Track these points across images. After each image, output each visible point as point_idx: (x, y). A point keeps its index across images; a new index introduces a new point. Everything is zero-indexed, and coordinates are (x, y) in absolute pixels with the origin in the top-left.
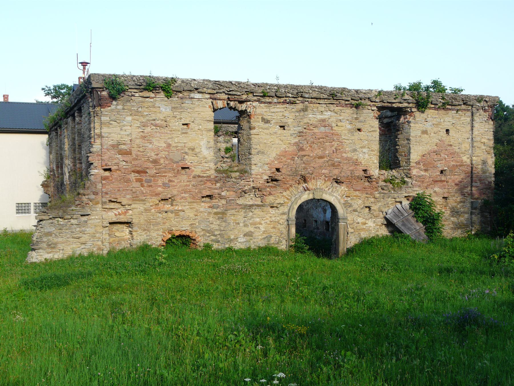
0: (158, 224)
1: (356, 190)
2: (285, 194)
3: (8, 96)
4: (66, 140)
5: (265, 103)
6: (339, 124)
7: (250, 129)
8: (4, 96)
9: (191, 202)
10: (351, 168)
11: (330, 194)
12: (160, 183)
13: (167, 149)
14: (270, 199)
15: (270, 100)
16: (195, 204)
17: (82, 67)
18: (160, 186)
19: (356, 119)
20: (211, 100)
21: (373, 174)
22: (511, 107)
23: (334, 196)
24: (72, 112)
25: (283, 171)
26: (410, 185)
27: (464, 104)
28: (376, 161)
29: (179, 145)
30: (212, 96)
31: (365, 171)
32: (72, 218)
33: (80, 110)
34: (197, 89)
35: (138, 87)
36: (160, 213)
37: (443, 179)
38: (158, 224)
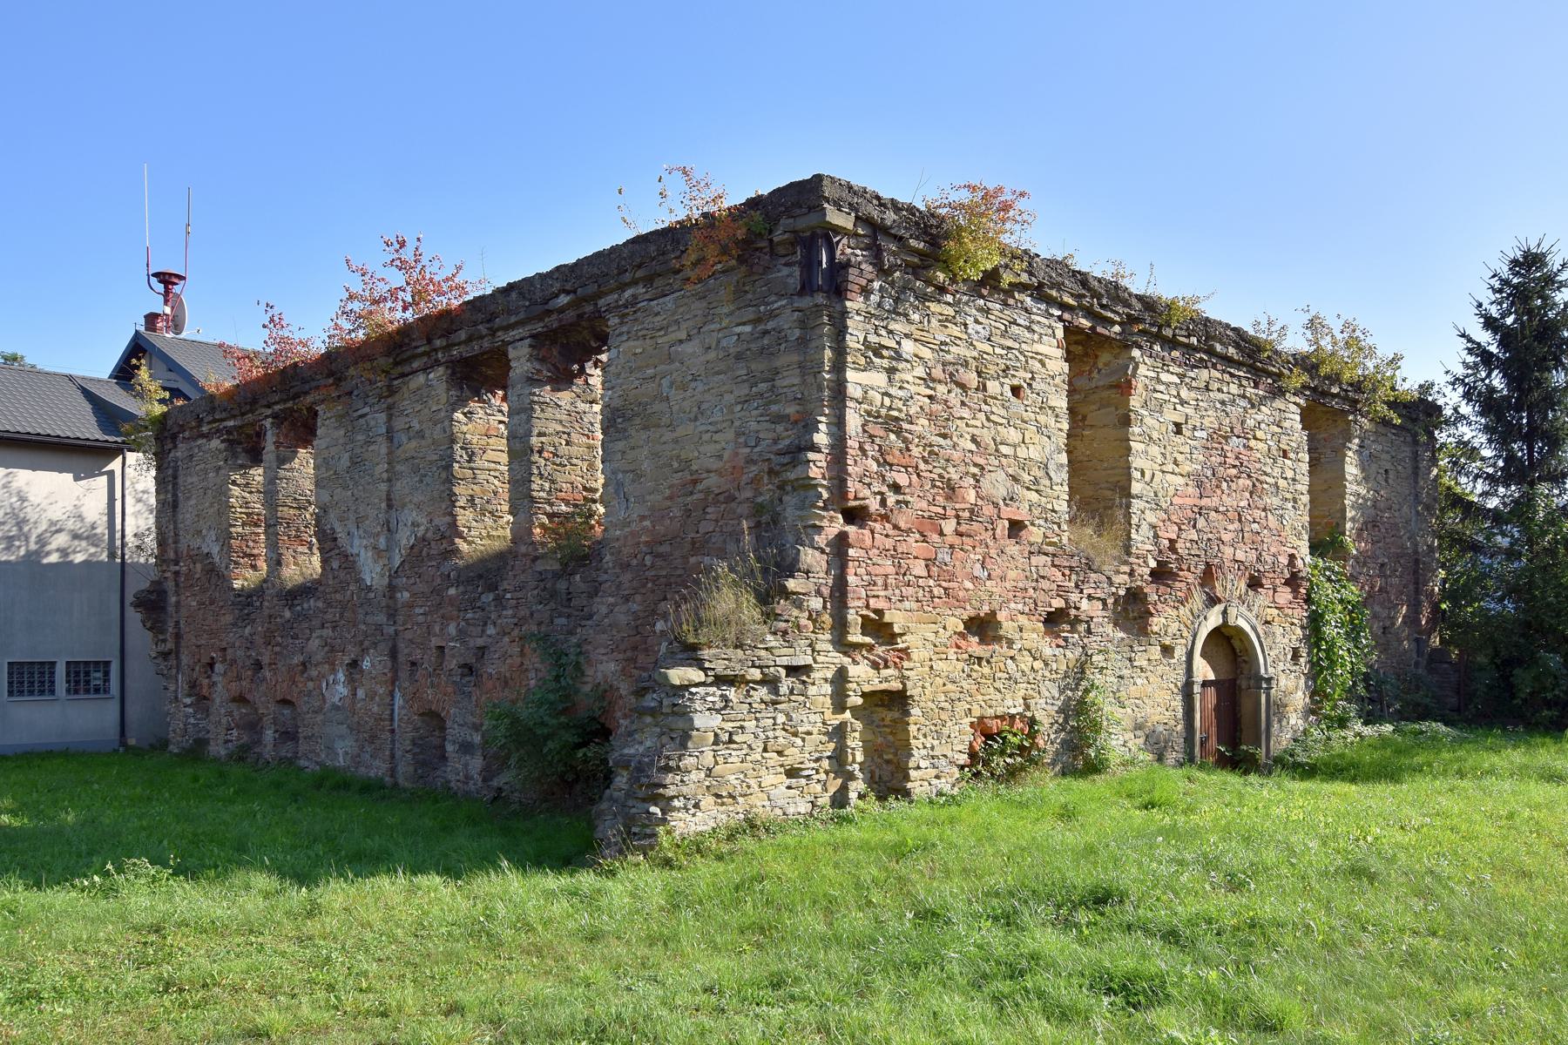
17: (161, 288)
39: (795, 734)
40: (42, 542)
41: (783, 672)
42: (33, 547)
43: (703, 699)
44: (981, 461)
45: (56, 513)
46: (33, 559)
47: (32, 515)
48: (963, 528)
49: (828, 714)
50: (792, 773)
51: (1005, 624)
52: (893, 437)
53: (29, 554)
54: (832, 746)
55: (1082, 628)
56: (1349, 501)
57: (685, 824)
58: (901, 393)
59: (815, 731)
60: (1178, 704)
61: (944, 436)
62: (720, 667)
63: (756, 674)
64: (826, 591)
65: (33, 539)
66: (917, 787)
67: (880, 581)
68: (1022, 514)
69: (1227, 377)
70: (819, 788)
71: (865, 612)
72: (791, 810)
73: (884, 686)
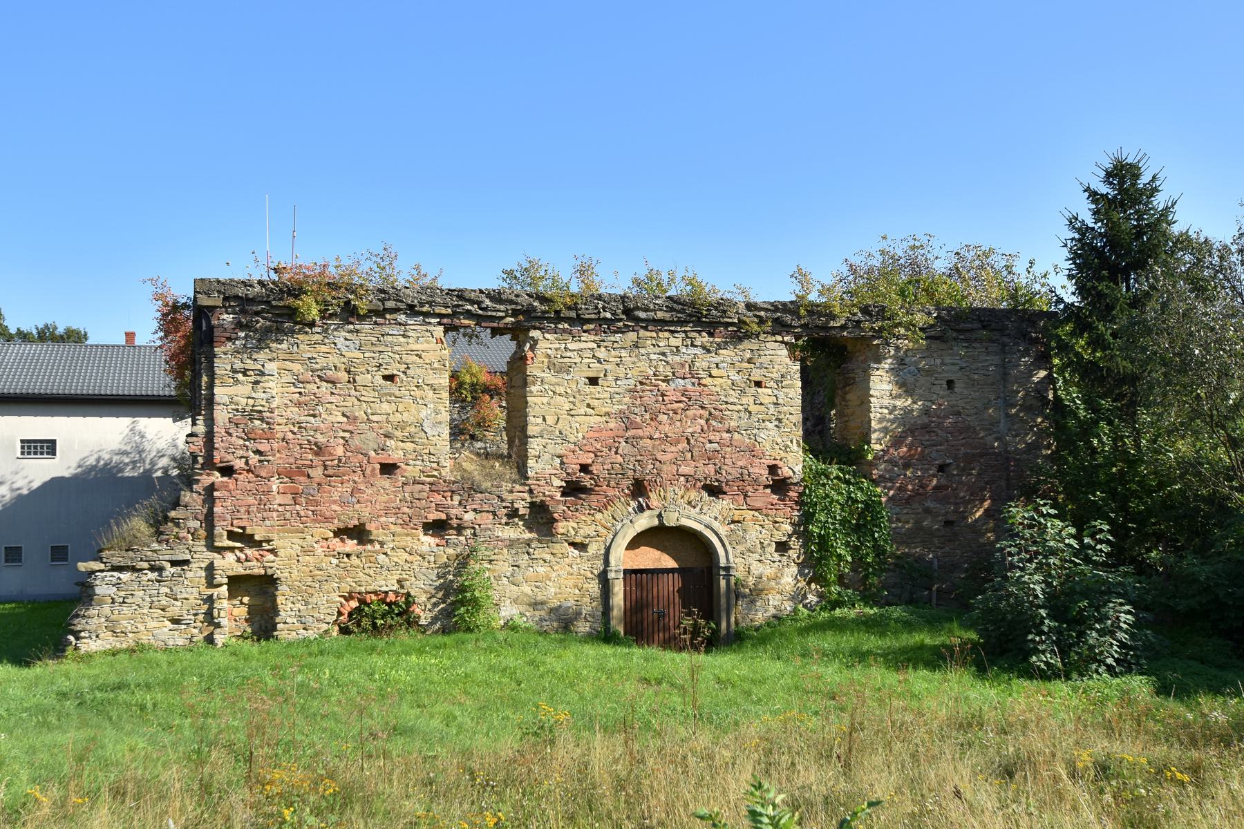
3: (133, 334)
18: (335, 502)
39: (176, 599)
40: (153, 463)
42: (148, 467)
43: (103, 578)
44: (350, 428)
45: (162, 444)
46: (148, 474)
47: (147, 446)
48: (330, 472)
49: (203, 588)
50: (176, 621)
51: (375, 532)
52: (257, 423)
53: (146, 471)
54: (206, 607)
55: (469, 532)
56: (876, 414)
57: (88, 645)
59: (191, 597)
60: (594, 587)
61: (314, 416)
62: (116, 561)
63: (146, 565)
64: (201, 517)
65: (148, 461)
66: (282, 632)
67: (243, 510)
68: (395, 456)
69: (667, 334)
70: (196, 631)
71: (230, 528)
72: (171, 643)
73: (248, 572)
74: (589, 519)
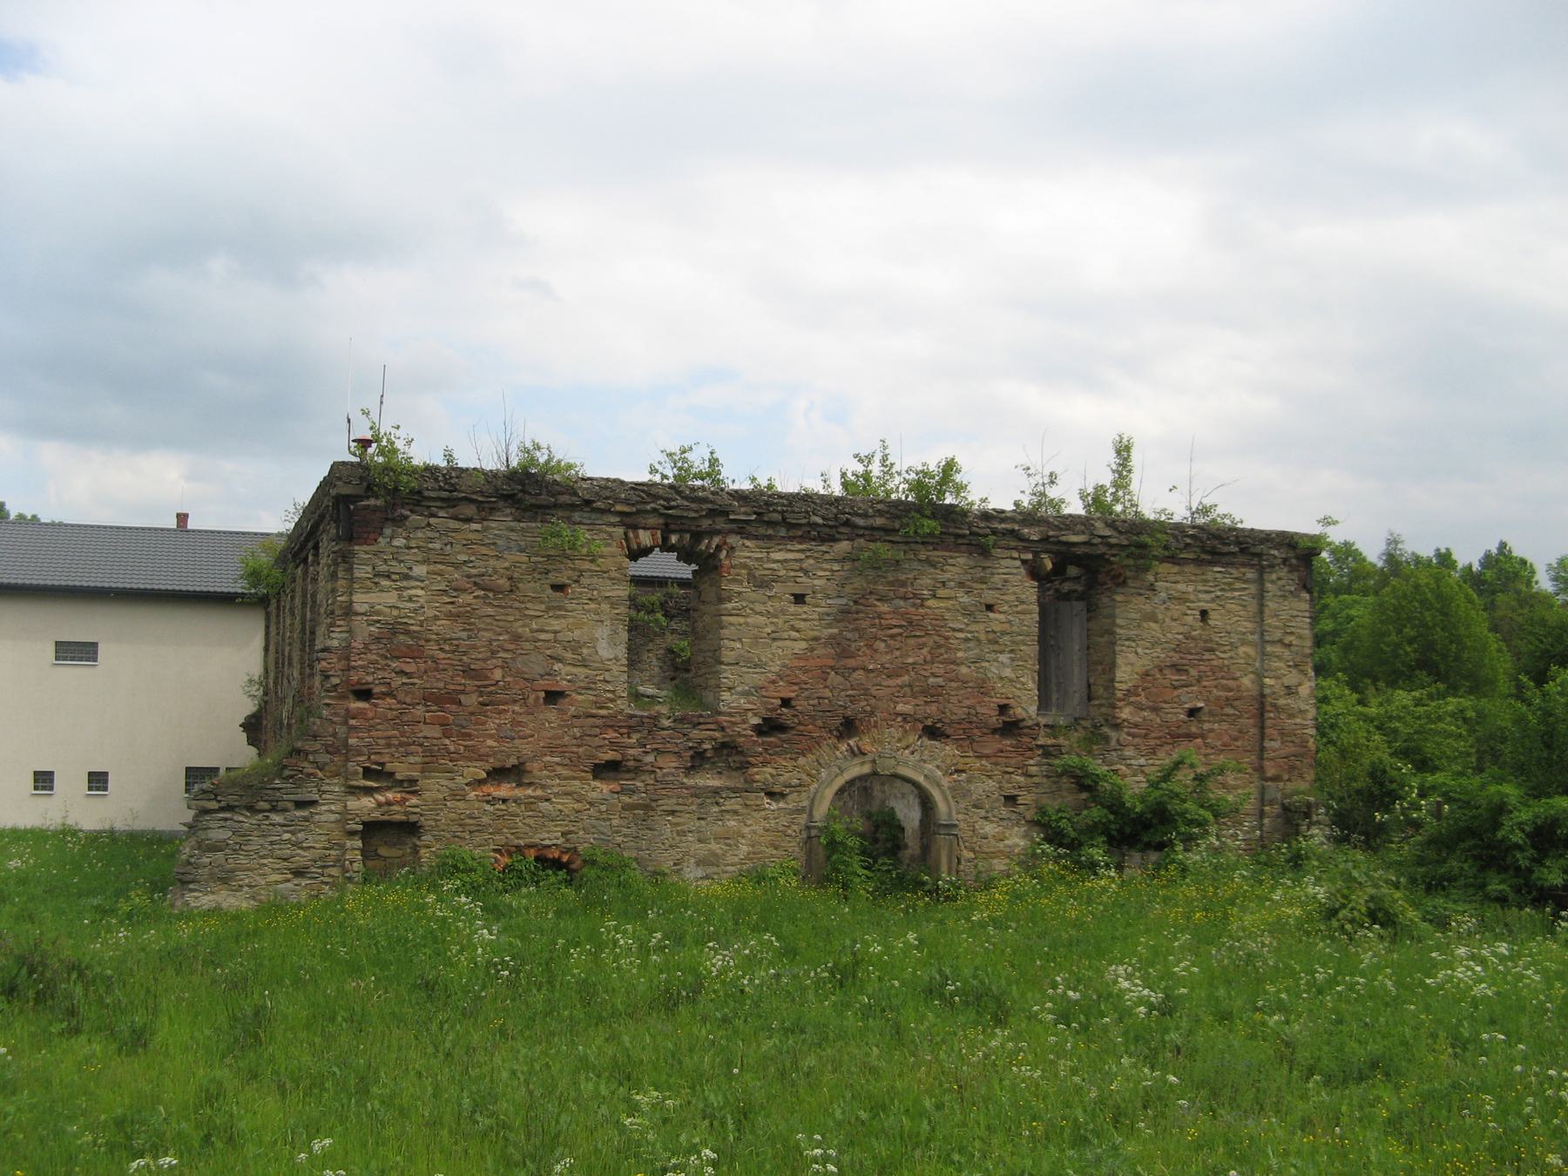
0: (481, 829)
1: (980, 757)
2: (802, 761)
4: (1076, 670)
5: (756, 538)
6: (940, 593)
7: (721, 600)
8: (178, 515)
9: (566, 778)
10: (967, 702)
11: (915, 768)
12: (491, 726)
13: (512, 647)
14: (763, 774)
15: (770, 532)
16: (577, 782)
19: (982, 581)
20: (621, 530)
21: (1024, 715)
22: (1544, 583)
23: (926, 764)
24: (303, 555)
25: (801, 705)
26: (1113, 743)
27: (1242, 551)
28: (1031, 685)
29: (543, 636)
30: (628, 520)
31: (1003, 709)
32: (274, 809)
33: (316, 547)
34: (588, 503)
35: (445, 494)
36: (488, 802)
37: (1194, 729)
38: (481, 829)
41: (290, 805)
58: (410, 605)
73: (386, 818)
74: (790, 764)
